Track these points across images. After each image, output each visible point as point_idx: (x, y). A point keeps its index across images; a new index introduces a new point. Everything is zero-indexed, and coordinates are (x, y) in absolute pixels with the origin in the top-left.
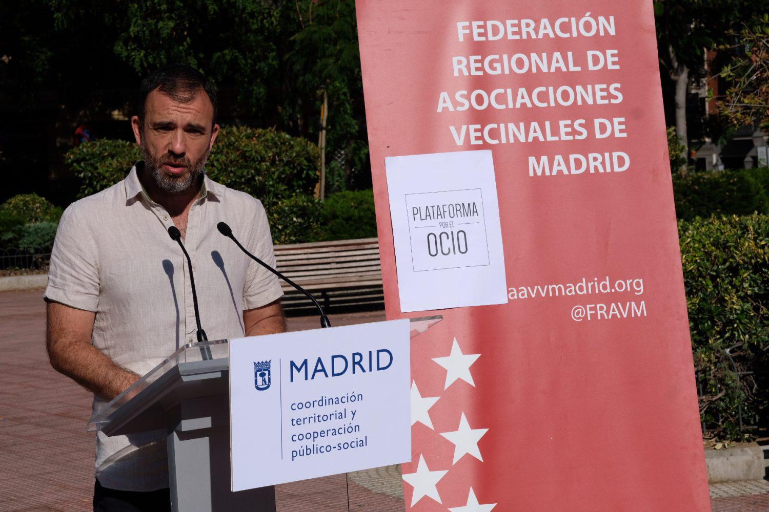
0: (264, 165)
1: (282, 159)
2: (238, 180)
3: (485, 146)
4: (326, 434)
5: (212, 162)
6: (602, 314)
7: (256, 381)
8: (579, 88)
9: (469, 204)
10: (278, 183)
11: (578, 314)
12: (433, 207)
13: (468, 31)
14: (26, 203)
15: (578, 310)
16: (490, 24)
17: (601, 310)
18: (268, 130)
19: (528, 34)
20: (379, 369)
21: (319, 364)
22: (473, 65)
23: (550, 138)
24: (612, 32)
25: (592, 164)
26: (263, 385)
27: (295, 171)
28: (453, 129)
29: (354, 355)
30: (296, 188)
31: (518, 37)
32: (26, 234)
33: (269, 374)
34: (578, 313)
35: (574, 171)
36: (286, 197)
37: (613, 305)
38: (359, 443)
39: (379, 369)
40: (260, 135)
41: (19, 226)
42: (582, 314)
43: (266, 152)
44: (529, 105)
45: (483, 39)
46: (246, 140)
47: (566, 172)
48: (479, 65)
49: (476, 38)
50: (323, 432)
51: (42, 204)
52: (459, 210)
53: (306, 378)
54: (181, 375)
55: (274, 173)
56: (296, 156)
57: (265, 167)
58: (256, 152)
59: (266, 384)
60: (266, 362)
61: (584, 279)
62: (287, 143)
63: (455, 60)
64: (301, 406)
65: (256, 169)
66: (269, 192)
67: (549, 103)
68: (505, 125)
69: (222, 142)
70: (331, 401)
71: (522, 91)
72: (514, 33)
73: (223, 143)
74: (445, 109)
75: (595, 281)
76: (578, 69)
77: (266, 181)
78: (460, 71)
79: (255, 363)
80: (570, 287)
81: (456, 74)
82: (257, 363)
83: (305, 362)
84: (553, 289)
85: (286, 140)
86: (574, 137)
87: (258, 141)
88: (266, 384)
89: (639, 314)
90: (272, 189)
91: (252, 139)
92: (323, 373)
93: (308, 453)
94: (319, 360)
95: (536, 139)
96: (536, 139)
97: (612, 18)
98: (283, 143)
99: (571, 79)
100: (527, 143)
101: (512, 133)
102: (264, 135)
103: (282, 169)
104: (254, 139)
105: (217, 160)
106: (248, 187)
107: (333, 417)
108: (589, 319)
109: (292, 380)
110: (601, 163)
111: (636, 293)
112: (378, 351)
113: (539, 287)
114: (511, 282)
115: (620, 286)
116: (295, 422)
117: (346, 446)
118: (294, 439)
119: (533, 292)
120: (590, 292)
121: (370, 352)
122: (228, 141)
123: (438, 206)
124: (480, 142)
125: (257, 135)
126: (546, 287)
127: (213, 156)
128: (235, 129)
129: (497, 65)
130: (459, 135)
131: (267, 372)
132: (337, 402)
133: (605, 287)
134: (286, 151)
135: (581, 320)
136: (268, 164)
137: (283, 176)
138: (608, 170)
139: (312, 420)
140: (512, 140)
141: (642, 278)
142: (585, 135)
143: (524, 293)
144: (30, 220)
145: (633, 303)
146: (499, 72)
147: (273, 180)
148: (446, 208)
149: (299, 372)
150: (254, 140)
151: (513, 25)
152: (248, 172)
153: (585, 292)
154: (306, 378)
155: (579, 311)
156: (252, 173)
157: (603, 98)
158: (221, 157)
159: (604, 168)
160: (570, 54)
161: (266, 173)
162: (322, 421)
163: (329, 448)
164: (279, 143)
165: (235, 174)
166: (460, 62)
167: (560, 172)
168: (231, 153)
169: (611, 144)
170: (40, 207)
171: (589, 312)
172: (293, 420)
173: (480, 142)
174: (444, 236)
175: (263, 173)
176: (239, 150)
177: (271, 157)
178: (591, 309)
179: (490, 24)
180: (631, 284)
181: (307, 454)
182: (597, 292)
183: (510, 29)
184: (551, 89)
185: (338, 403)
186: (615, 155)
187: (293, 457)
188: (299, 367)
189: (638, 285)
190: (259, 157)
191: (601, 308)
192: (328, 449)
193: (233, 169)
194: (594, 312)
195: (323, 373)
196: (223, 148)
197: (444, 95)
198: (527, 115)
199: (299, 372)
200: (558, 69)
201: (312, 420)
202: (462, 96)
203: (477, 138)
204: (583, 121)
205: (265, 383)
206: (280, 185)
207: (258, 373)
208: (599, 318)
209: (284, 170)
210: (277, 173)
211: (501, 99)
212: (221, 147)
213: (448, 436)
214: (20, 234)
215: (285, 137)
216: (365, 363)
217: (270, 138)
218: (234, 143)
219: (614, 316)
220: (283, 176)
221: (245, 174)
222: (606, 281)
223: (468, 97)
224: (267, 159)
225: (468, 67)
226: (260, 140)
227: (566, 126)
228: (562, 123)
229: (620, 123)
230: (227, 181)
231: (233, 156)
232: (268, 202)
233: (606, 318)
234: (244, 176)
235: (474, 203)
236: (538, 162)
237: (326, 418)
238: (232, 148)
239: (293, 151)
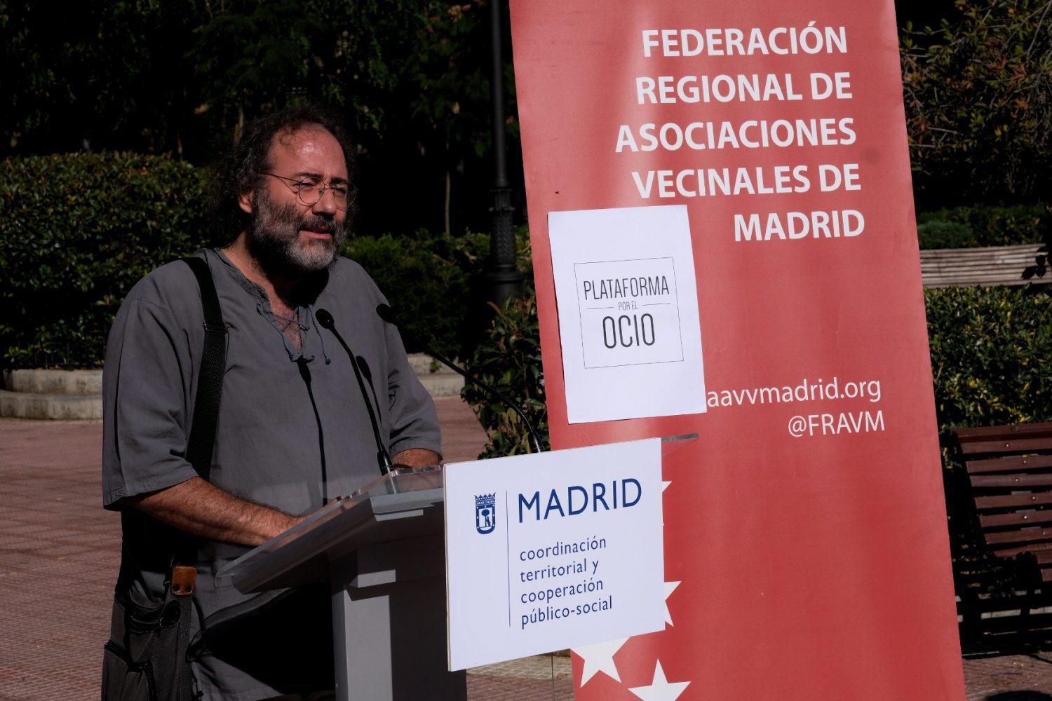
0: (159, 206)
1: (184, 198)
2: (123, 226)
3: (679, 200)
5: (88, 199)
6: (828, 428)
7: (478, 521)
8: (800, 124)
9: (657, 278)
10: (178, 231)
11: (798, 427)
12: (610, 281)
13: (656, 43)
15: (797, 422)
18: (163, 157)
19: (735, 48)
20: (625, 505)
22: (664, 90)
23: (762, 190)
24: (843, 48)
25: (816, 226)
26: (486, 526)
27: (201, 215)
28: (636, 175)
29: (595, 486)
30: (200, 238)
31: (721, 53)
33: (494, 513)
34: (797, 426)
35: (793, 236)
36: (187, 250)
37: (842, 415)
38: (602, 605)
40: (151, 163)
42: (803, 428)
43: (162, 187)
44: (736, 145)
45: (676, 54)
46: (133, 170)
47: (782, 236)
48: (671, 89)
49: (668, 53)
52: (644, 286)
53: (538, 518)
55: (172, 216)
56: (202, 194)
57: (160, 208)
58: (148, 187)
59: (489, 526)
60: (490, 495)
61: (805, 381)
62: (189, 176)
63: (639, 81)
64: (533, 555)
65: (147, 211)
66: (166, 242)
67: (761, 143)
69: (99, 173)
71: (726, 125)
72: (716, 47)
73: (102, 174)
74: (626, 148)
75: (819, 384)
76: (799, 97)
77: (161, 227)
78: (646, 97)
79: (476, 497)
80: (788, 391)
81: (641, 101)
82: (478, 496)
83: (537, 496)
84: (766, 394)
85: (188, 171)
87: (150, 172)
89: (875, 428)
90: (170, 239)
91: (142, 168)
92: (558, 510)
94: (554, 493)
95: (744, 191)
96: (744, 191)
97: (842, 30)
98: (185, 176)
100: (732, 196)
101: (714, 181)
102: (157, 164)
103: (184, 211)
104: (144, 168)
105: (95, 198)
106: (137, 236)
107: (571, 569)
108: (811, 434)
109: (521, 521)
110: (827, 225)
111: (872, 400)
113: (747, 391)
114: (713, 382)
115: (851, 390)
119: (739, 397)
120: (813, 398)
121: (615, 482)
122: (109, 171)
123: (617, 280)
124: (672, 194)
125: (147, 164)
126: (756, 390)
127: (89, 191)
128: (117, 155)
129: (695, 90)
130: (645, 185)
132: (575, 550)
133: (832, 391)
134: (189, 187)
135: (801, 435)
136: (165, 204)
137: (185, 221)
138: (837, 234)
139: (546, 573)
140: (713, 192)
141: (879, 380)
143: (729, 398)
145: (867, 413)
146: (696, 99)
147: (171, 226)
148: (627, 284)
149: (529, 509)
150: (143, 171)
151: (715, 37)
152: (137, 214)
153: (806, 397)
154: (538, 518)
155: (798, 424)
156: (142, 216)
157: (830, 137)
158: (100, 193)
159: (832, 231)
160: (788, 77)
161: (162, 216)
163: (567, 612)
164: (179, 176)
165: (119, 216)
166: (646, 85)
167: (775, 236)
168: (114, 187)
169: (840, 200)
171: (811, 425)
172: (522, 574)
173: (672, 194)
174: (624, 321)
175: (157, 217)
176: (125, 185)
177: (169, 195)
178: (814, 421)
179: (685, 33)
180: (865, 388)
181: (540, 620)
182: (822, 397)
183: (711, 42)
184: (764, 124)
185: (577, 551)
186: (846, 214)
187: (523, 624)
188: (529, 503)
189: (874, 389)
190: (152, 194)
191: (828, 420)
193: (116, 210)
194: (817, 425)
195: (557, 511)
196: (102, 181)
197: (624, 129)
198: (731, 159)
199: (529, 509)
200: (773, 96)
201: (546, 573)
202: (649, 131)
203: (668, 189)
204: (804, 168)
205: (489, 523)
206: (181, 233)
207: (481, 511)
208: (825, 433)
209: (186, 213)
210: (176, 218)
212: (99, 179)
215: (186, 167)
216: (608, 497)
217: (165, 167)
218: (117, 174)
219: (844, 430)
220: (185, 221)
221: (133, 217)
222: (833, 383)
223: (656, 133)
224: (163, 197)
225: (656, 91)
226: (152, 170)
227: (783, 174)
228: (778, 170)
229: (852, 172)
230: (109, 227)
231: (116, 193)
232: (164, 256)
233: (834, 432)
234: (131, 221)
235: (664, 277)
236: (747, 222)
237: (563, 571)
238: (114, 180)
239: (198, 186)
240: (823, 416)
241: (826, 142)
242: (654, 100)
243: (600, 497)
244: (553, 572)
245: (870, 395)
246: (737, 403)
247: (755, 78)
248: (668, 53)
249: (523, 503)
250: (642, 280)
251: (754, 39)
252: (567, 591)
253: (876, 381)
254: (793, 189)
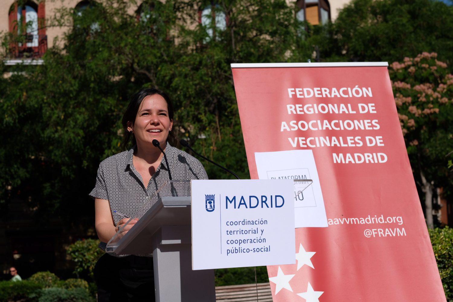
3: (308, 148)
4: (246, 242)
6: (381, 234)
7: (206, 207)
8: (356, 122)
9: (302, 176)
11: (368, 233)
13: (294, 93)
14: (43, 277)
15: (368, 232)
16: (305, 90)
17: (380, 232)
19: (326, 95)
20: (276, 206)
21: (242, 200)
23: (343, 145)
24: (370, 95)
25: (367, 159)
28: (290, 139)
29: (262, 197)
32: (43, 295)
33: (214, 203)
34: (368, 233)
35: (357, 162)
37: (387, 229)
38: (265, 249)
39: (276, 206)
41: (39, 290)
42: (370, 234)
50: (244, 240)
51: (53, 277)
53: (235, 208)
54: (163, 205)
60: (212, 195)
63: (288, 106)
64: (232, 223)
68: (318, 138)
70: (249, 222)
74: (285, 130)
75: (375, 217)
76: (355, 112)
78: (292, 112)
79: (206, 195)
81: (290, 113)
83: (234, 198)
84: (353, 220)
86: (356, 145)
88: (212, 208)
89: (402, 235)
93: (236, 252)
94: (242, 198)
97: (370, 89)
99: (352, 117)
100: (331, 147)
107: (251, 232)
109: (227, 208)
111: (399, 224)
112: (276, 196)
116: (228, 233)
117: (258, 250)
118: (228, 243)
119: (342, 221)
121: (271, 196)
123: (285, 177)
124: (305, 146)
129: (311, 109)
131: (212, 201)
133: (381, 220)
138: (376, 162)
139: (238, 232)
142: (361, 144)
144: (46, 287)
145: (398, 229)
146: (312, 112)
149: (231, 203)
153: (370, 222)
154: (235, 208)
157: (369, 126)
160: (349, 105)
162: (244, 233)
163: (248, 250)
169: (375, 149)
170: (51, 279)
171: (374, 233)
173: (305, 146)
178: (375, 231)
179: (305, 90)
180: (396, 219)
181: (236, 253)
186: (379, 154)
187: (228, 253)
188: (231, 200)
189: (399, 220)
192: (248, 251)
194: (376, 233)
195: (244, 205)
197: (284, 123)
201: (238, 232)
202: (294, 123)
203: (303, 144)
205: (212, 207)
207: (208, 201)
211: (314, 125)
213: (301, 295)
214: (40, 295)
216: (269, 202)
219: (388, 235)
223: (297, 124)
225: (295, 109)
227: (351, 140)
228: (349, 138)
237: (247, 232)
240: (379, 230)
241: (367, 128)
242: (295, 113)
243: (265, 202)
244: (242, 232)
245: (398, 222)
246: (341, 223)
247: (336, 105)
248: (298, 96)
249: (228, 201)
250: (302, 199)
251: (334, 91)
252: (249, 241)
253: (400, 217)
254: (356, 145)
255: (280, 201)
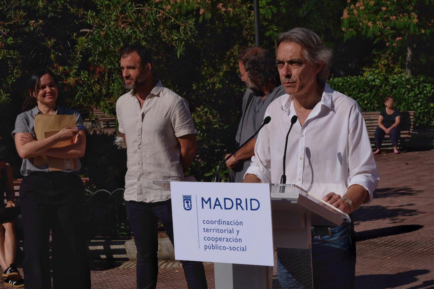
64: (208, 222)
216: (243, 204)
237: (222, 231)
255: (255, 205)
